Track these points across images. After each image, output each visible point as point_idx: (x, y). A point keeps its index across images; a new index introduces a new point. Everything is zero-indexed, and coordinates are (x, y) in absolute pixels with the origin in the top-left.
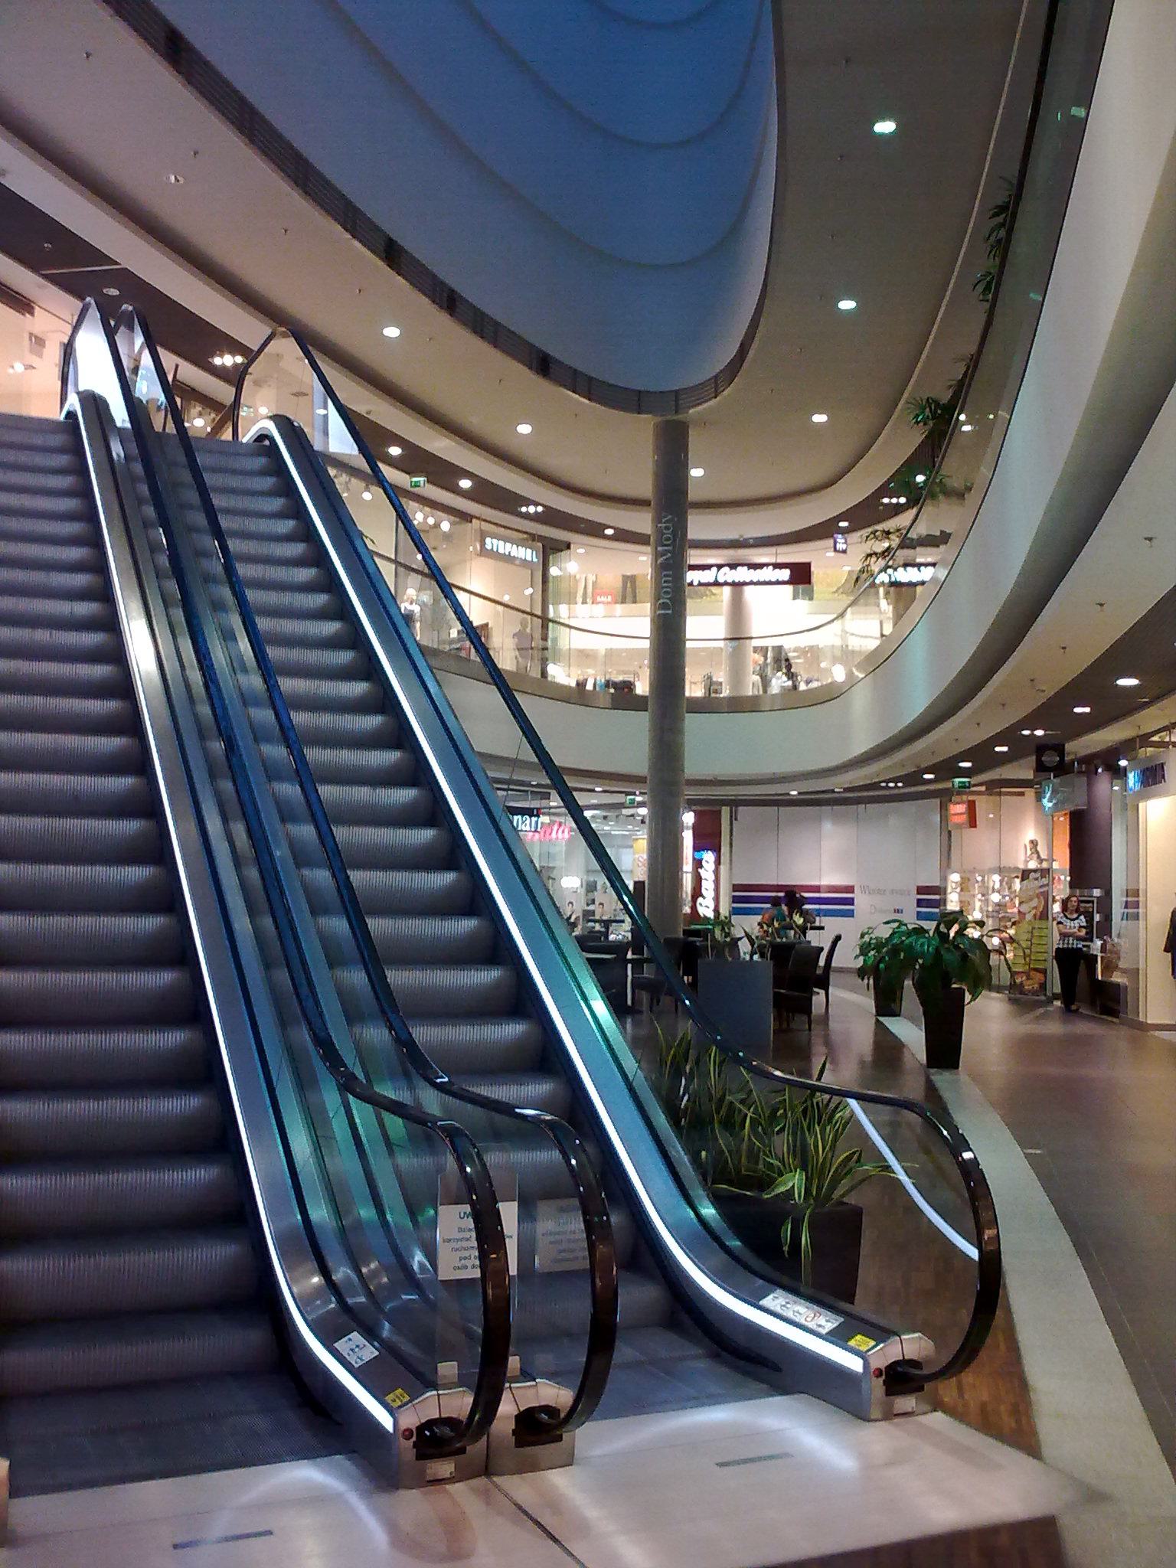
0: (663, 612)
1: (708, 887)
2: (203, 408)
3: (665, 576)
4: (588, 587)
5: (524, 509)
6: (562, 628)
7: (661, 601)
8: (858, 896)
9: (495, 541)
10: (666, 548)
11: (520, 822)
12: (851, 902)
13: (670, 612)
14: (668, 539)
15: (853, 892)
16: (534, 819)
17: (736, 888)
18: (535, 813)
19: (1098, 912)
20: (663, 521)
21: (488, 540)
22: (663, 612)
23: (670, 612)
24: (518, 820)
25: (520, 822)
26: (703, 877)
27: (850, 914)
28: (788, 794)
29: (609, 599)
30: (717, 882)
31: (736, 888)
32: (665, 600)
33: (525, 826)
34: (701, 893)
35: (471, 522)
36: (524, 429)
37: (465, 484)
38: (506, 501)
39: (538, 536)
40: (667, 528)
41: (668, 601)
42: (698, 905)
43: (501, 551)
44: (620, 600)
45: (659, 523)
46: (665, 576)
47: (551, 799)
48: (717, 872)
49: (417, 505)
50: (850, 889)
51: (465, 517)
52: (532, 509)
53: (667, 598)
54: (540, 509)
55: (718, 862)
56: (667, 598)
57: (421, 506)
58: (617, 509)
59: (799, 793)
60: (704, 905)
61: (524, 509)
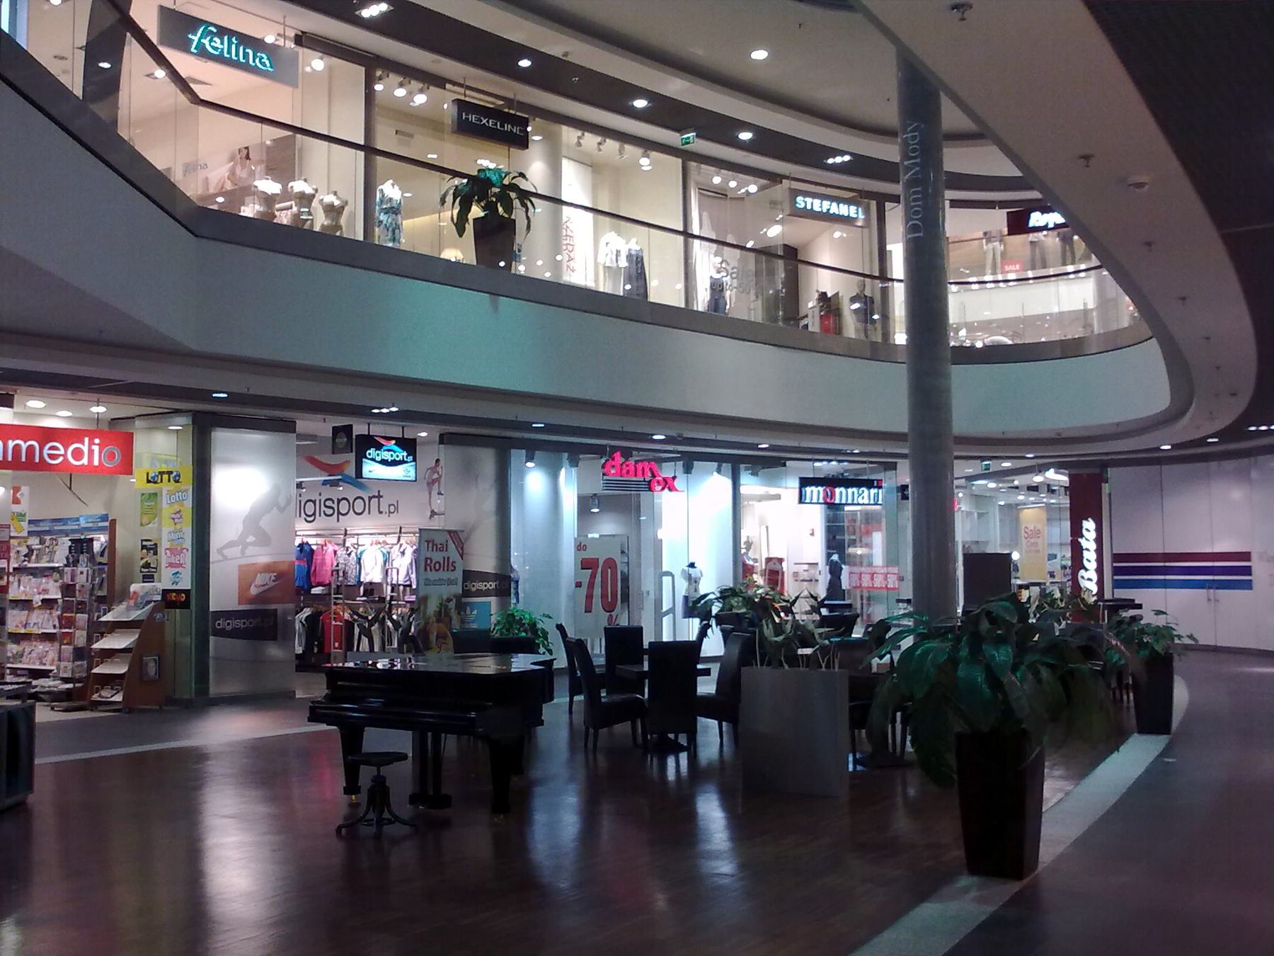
0: (912, 236)
1: (1090, 557)
2: (404, 78)
3: (915, 193)
4: (996, 255)
5: (830, 161)
6: (820, 270)
7: (911, 223)
8: (1255, 564)
9: (809, 200)
10: (913, 161)
11: (856, 495)
12: (1247, 571)
13: (921, 234)
14: (914, 150)
15: (1249, 560)
16: (873, 491)
17: (1117, 557)
18: (875, 484)
19: (731, 610)
20: (909, 129)
21: (800, 199)
22: (912, 236)
23: (921, 234)
24: (841, 493)
25: (856, 495)
26: (1084, 548)
27: (1248, 585)
28: (1158, 449)
29: (1018, 267)
30: (1099, 551)
31: (1117, 557)
32: (914, 222)
33: (863, 498)
34: (1083, 565)
35: (781, 183)
36: (760, 55)
37: (745, 136)
38: (812, 155)
39: (517, 102)
40: (914, 138)
41: (917, 222)
42: (1079, 578)
43: (817, 208)
44: (1029, 267)
45: (904, 134)
46: (915, 193)
47: (441, 446)
48: (1099, 540)
49: (713, 169)
50: (1246, 556)
51: (775, 178)
52: (838, 160)
53: (917, 219)
54: (847, 158)
55: (1099, 530)
56: (917, 219)
57: (718, 169)
58: (541, 25)
59: (1174, 447)
60: (1086, 578)
61: (830, 161)
